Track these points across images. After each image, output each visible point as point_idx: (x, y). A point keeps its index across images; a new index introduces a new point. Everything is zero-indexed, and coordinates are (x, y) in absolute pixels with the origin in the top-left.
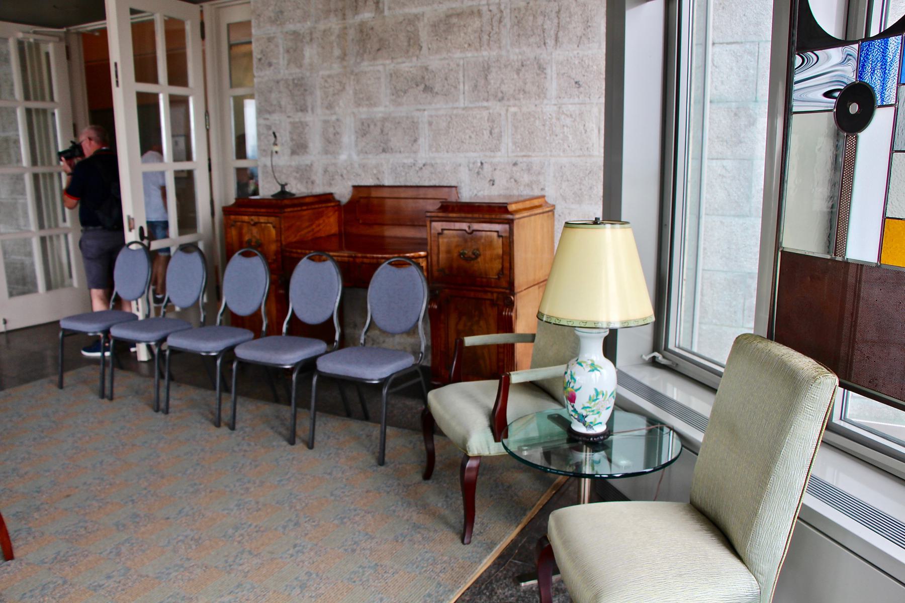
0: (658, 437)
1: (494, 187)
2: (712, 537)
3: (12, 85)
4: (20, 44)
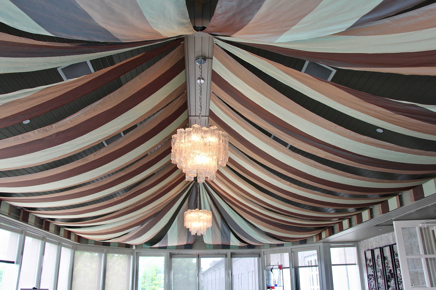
3: (418, 247)
4: (421, 229)
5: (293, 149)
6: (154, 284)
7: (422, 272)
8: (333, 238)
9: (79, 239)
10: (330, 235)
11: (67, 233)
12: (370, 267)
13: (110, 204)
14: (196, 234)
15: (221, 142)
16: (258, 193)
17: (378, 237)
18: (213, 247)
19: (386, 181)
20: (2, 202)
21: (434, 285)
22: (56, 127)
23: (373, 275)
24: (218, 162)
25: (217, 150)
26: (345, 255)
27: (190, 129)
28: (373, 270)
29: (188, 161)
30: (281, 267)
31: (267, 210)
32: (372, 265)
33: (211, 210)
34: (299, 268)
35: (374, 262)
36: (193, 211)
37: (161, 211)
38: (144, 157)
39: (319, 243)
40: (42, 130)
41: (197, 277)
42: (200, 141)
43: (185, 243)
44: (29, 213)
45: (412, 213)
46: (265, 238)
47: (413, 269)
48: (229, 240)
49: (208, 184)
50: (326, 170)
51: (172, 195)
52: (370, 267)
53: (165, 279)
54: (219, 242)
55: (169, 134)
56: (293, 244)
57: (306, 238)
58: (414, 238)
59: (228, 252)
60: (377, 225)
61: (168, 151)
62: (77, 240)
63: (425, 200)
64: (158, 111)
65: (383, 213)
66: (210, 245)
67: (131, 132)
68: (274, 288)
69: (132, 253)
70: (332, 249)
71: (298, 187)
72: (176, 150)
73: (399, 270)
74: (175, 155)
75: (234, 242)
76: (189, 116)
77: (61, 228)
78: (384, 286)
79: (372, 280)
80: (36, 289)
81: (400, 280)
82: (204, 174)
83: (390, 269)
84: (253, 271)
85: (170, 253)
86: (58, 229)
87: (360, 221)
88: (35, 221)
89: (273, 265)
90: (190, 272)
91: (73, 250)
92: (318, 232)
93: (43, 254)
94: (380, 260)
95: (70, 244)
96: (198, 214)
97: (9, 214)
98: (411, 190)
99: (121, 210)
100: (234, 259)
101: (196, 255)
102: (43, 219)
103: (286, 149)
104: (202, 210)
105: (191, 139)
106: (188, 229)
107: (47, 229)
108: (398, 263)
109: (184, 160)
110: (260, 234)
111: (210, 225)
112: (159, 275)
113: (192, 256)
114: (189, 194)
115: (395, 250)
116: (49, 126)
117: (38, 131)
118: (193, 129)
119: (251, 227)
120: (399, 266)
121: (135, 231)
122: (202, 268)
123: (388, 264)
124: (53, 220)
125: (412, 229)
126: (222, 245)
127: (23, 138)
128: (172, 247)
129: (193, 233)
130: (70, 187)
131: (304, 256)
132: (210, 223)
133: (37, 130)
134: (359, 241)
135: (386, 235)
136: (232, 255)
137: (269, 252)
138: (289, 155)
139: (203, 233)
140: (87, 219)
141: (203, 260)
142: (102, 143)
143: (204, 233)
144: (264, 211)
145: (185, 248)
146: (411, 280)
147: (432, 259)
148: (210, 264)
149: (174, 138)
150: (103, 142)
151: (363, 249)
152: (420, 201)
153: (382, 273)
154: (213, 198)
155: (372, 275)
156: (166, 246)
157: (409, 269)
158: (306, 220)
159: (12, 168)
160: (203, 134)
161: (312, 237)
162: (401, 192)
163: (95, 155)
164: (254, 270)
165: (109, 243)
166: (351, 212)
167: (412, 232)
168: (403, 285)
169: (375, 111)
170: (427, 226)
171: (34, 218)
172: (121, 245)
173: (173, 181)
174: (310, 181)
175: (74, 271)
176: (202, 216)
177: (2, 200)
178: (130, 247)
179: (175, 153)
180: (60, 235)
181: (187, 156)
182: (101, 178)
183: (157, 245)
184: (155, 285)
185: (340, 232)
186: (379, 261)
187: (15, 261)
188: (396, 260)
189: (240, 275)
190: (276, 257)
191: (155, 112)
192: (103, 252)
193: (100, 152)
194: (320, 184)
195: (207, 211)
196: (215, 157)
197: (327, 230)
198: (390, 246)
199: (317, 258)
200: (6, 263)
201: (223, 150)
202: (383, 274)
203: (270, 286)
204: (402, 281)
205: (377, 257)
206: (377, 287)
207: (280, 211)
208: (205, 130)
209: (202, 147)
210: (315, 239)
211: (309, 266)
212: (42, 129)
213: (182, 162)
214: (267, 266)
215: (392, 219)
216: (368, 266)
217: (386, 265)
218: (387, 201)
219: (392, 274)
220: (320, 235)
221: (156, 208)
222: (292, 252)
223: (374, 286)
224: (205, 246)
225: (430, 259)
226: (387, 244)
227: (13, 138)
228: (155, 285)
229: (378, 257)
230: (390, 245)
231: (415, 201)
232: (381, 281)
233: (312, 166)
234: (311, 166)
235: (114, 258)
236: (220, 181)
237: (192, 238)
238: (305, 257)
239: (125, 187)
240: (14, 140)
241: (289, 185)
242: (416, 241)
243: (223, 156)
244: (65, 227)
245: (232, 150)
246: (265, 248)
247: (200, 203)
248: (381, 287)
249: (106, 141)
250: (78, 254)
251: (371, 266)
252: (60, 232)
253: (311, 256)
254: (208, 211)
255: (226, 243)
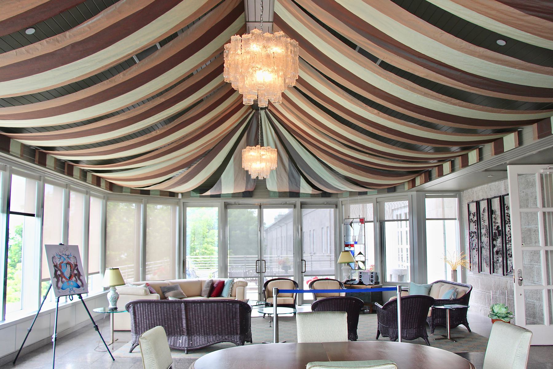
0: (243, 256)
1: (118, 338)
2: (318, 313)
3: (536, 198)
4: (541, 176)
5: (385, 66)
6: (206, 242)
7: (536, 228)
8: (429, 185)
9: (111, 186)
10: (426, 181)
11: (95, 178)
12: (473, 223)
13: (147, 140)
14: (257, 177)
15: (289, 53)
16: (336, 125)
17: (486, 186)
18: (278, 195)
19: (503, 111)
20: (12, 141)
21: (551, 284)
22: (70, 36)
23: (477, 232)
24: (286, 81)
25: (284, 64)
26: (443, 208)
27: (248, 35)
28: (476, 227)
29: (246, 79)
30: (362, 221)
31: (347, 148)
32: (475, 220)
33: (276, 147)
34: (385, 222)
35: (478, 217)
36: (253, 148)
37: (212, 150)
38: (188, 77)
39: (412, 191)
40: (51, 40)
41: (259, 232)
42: (260, 51)
43: (243, 190)
44: (46, 154)
45: (533, 155)
46: (343, 184)
47: (526, 226)
48: (298, 186)
49: (270, 108)
50: (425, 95)
51: (226, 128)
52: (473, 223)
53: (219, 236)
54: (286, 189)
55: (220, 46)
56: (380, 192)
57: (396, 185)
58: (532, 188)
59: (298, 201)
60: (486, 170)
61: (220, 70)
62: (108, 187)
63: (551, 137)
64: (205, 14)
65: (496, 153)
66: (274, 192)
67: (171, 43)
68: (353, 246)
69: (178, 204)
70: (427, 200)
71: (388, 117)
72: (229, 65)
73: (508, 226)
74: (228, 71)
75: (305, 189)
76: (246, 22)
77: (88, 173)
78: (488, 245)
79: (474, 238)
80: (63, 245)
81: (509, 238)
82: (266, 95)
83: (498, 225)
84: (327, 227)
85: (225, 202)
86: (84, 174)
87: (465, 163)
88: (54, 164)
89: (353, 219)
90: (251, 227)
91: (105, 201)
92: (410, 177)
93: (69, 207)
94: (486, 214)
95: (100, 194)
96: (260, 152)
97: (22, 156)
98: (535, 125)
99: (161, 148)
100: (306, 211)
101: (258, 205)
102: (64, 161)
103: (376, 66)
104: (265, 147)
105: (249, 49)
106: (247, 171)
107: (70, 174)
108: (508, 218)
109: (241, 77)
110: (338, 179)
111: (275, 166)
112: (211, 231)
113: (252, 206)
114: (248, 128)
115: (506, 202)
116: (61, 35)
117: (47, 42)
118: (252, 36)
119: (326, 170)
120: (510, 221)
121: (181, 175)
122: (265, 224)
123: (495, 219)
124: (77, 162)
125: (530, 177)
126: (290, 192)
127: (28, 52)
128: (226, 195)
129: (253, 177)
130: (94, 119)
131: (393, 209)
132: (274, 164)
133: (46, 41)
134: (463, 190)
135: (497, 183)
136: (302, 206)
137: (348, 202)
138: (377, 73)
139: (266, 176)
140: (119, 161)
141: (266, 211)
142: (132, 58)
143: (267, 176)
144: (344, 149)
145: (243, 197)
146: (522, 238)
147: (551, 212)
148: (275, 219)
149: (227, 48)
150: (133, 56)
151: (466, 201)
152: (545, 139)
153: (487, 230)
154: (278, 132)
155: (475, 232)
156: (220, 194)
157: (521, 225)
158: (397, 161)
159: (19, 93)
160: (265, 42)
161: (403, 184)
162: (521, 127)
163: (124, 75)
164: (329, 225)
165: (149, 191)
166: (455, 152)
167: (529, 180)
168: (511, 245)
169: (498, 11)
170: (550, 172)
171: (53, 161)
172: (163, 193)
173: (227, 110)
174: (405, 110)
175: (107, 228)
176: (264, 155)
177: (12, 138)
178: (175, 196)
179: (229, 68)
180: (87, 182)
181: (244, 71)
182: (133, 106)
183: (208, 193)
184: (208, 243)
185: (439, 177)
186: (485, 216)
187: (35, 214)
188: (506, 215)
189: (312, 232)
190: (358, 208)
191: (201, 16)
192: (141, 202)
193: (131, 71)
194: (417, 113)
195: (271, 148)
196: (281, 73)
197: (423, 175)
198: (500, 197)
199: (408, 211)
200: (25, 215)
201: (291, 64)
202: (488, 231)
203: (348, 244)
204: (511, 240)
205: (483, 211)
206: (479, 247)
207: (363, 149)
208: (268, 37)
209: (264, 59)
210: (406, 186)
211: (397, 220)
212: (52, 39)
213: (238, 80)
214: (345, 219)
215: (506, 163)
216: (471, 221)
217: (493, 220)
218: (502, 139)
219: (499, 232)
220: (413, 181)
221: (205, 146)
222: (377, 202)
223: (476, 245)
224: (268, 194)
225: (549, 213)
226: (496, 195)
227: (13, 52)
228: (208, 243)
229: (484, 210)
230: (501, 196)
231: (538, 139)
232: (485, 239)
233: (408, 88)
234: (407, 88)
235: (156, 211)
236: (287, 109)
237: (253, 184)
238: (393, 210)
239: (165, 118)
240: (16, 54)
241: (377, 114)
242: (534, 191)
243: (291, 72)
244: (92, 172)
245: (303, 68)
246: (344, 196)
247: (262, 140)
248: (484, 247)
249: (137, 56)
250: (112, 206)
251: (474, 221)
252: (86, 178)
253: (401, 208)
254: (272, 149)
255: (294, 190)
